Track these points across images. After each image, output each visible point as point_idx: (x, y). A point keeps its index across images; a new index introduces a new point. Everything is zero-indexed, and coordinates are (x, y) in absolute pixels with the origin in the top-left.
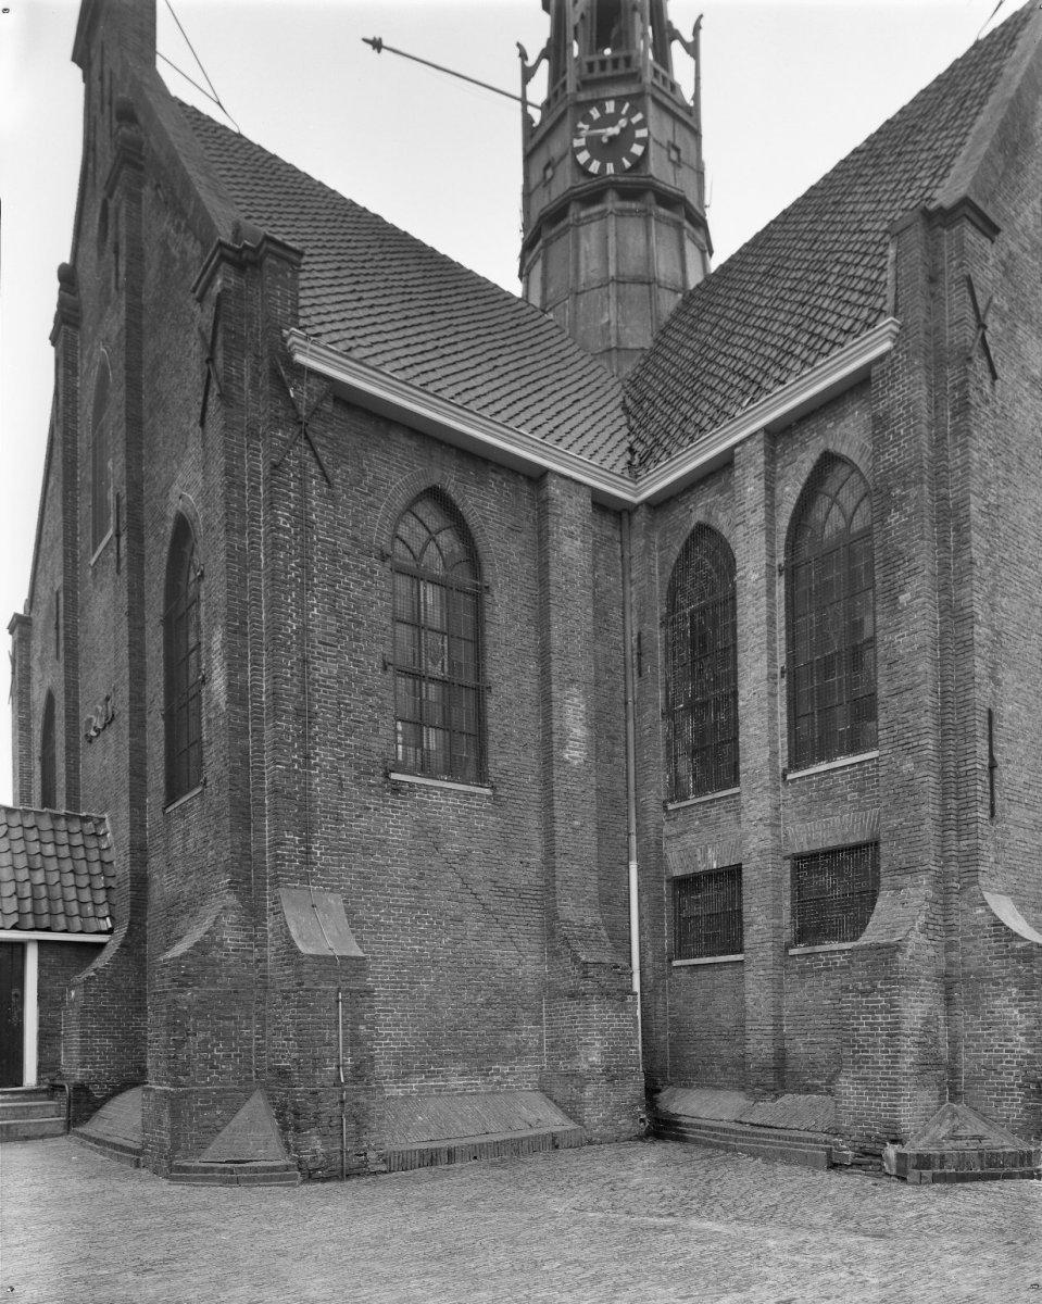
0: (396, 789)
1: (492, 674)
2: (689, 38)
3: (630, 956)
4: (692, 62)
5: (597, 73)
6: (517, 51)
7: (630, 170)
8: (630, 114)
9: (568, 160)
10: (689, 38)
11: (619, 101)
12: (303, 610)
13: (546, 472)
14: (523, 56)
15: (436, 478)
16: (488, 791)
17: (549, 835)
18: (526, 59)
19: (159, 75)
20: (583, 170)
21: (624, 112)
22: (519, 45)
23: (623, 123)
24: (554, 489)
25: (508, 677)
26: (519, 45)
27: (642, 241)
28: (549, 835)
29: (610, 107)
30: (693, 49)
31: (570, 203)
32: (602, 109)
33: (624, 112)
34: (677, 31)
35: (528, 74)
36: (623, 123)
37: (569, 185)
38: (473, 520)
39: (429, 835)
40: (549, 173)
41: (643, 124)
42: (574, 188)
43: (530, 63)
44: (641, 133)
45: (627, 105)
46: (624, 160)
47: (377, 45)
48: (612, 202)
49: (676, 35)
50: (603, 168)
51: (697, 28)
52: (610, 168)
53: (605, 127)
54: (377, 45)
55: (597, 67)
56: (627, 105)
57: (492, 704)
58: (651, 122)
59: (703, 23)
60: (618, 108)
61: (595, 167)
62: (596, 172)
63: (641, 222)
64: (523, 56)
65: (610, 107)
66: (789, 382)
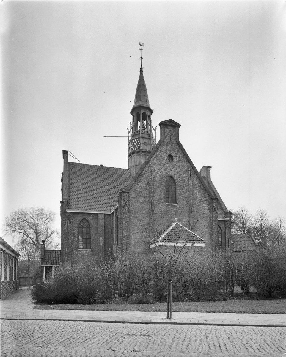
0: (79, 251)
1: (91, 237)
4: (155, 133)
7: (138, 149)
8: (138, 140)
11: (137, 139)
12: (67, 235)
15: (84, 217)
19: (181, 144)
24: (99, 215)
25: (93, 237)
27: (139, 159)
32: (134, 140)
38: (89, 221)
39: (83, 255)
41: (140, 142)
44: (139, 143)
47: (105, 137)
48: (135, 154)
49: (153, 127)
50: (135, 149)
51: (156, 128)
54: (105, 137)
57: (91, 240)
58: (141, 141)
59: (157, 127)
60: (136, 140)
63: (139, 156)
65: (135, 140)
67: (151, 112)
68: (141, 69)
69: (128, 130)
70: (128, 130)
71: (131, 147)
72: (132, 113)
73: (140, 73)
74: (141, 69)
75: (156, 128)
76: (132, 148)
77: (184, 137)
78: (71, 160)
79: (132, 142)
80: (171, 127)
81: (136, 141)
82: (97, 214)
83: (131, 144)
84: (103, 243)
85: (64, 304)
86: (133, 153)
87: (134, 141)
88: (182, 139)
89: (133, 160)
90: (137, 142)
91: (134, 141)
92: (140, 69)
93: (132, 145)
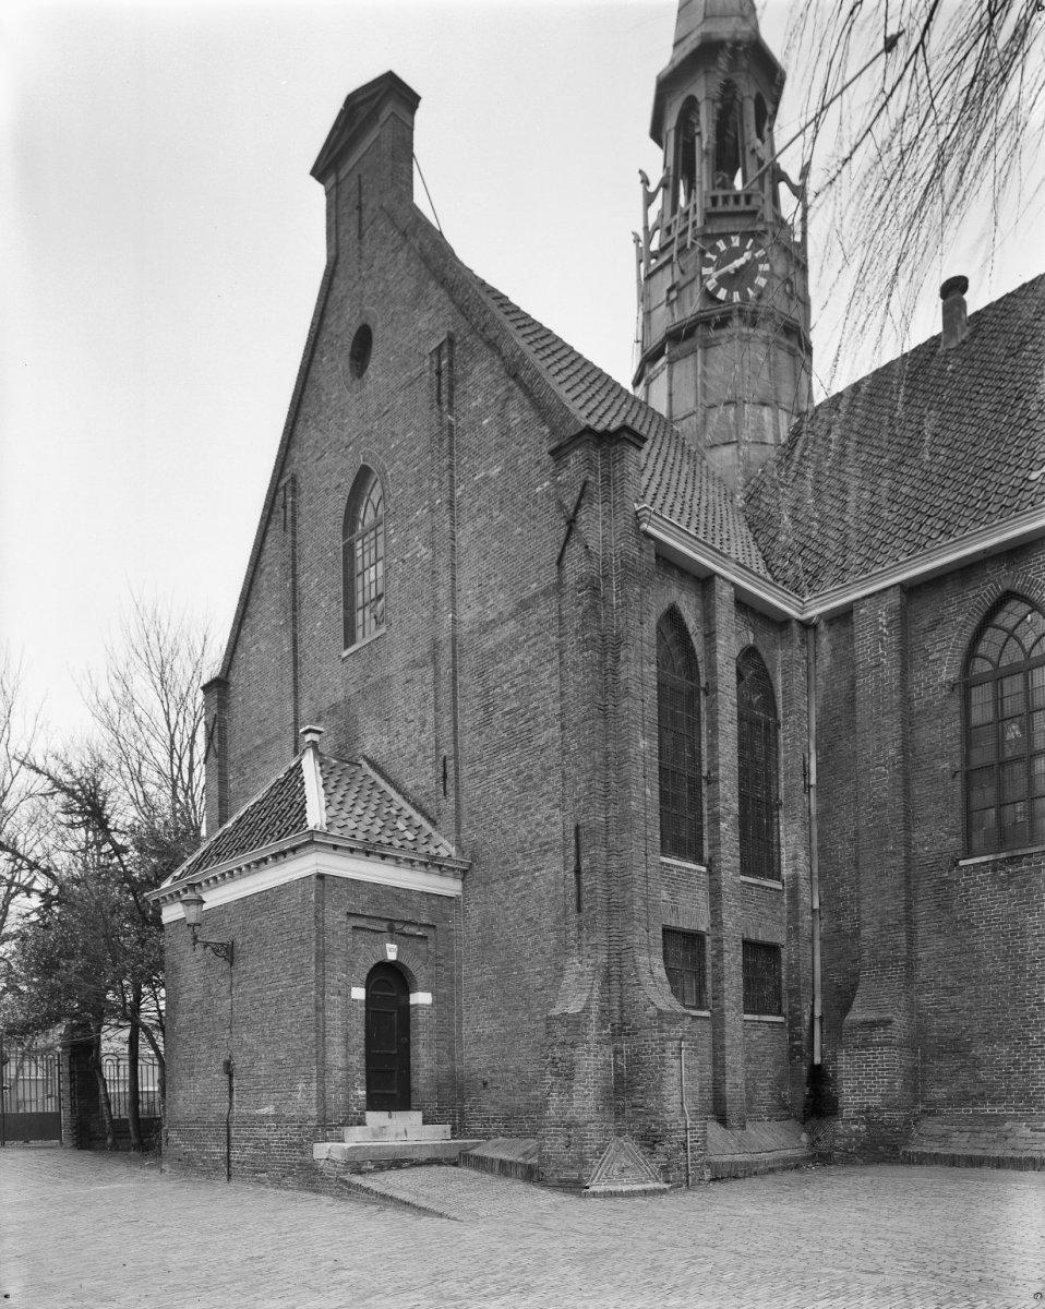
2: (795, 179)
3: (428, 894)
5: (720, 207)
6: (639, 178)
9: (697, 287)
10: (796, 180)
13: (715, 574)
14: (646, 182)
16: (704, 869)
17: (296, 711)
18: (648, 184)
20: (710, 296)
21: (748, 247)
22: (641, 172)
23: (747, 255)
26: (641, 172)
28: (296, 711)
29: (736, 241)
30: (799, 192)
31: (696, 327)
32: (728, 242)
33: (748, 247)
34: (785, 174)
35: (649, 199)
36: (747, 255)
37: (697, 309)
40: (674, 295)
41: (763, 260)
42: (703, 311)
43: (652, 189)
45: (751, 241)
46: (749, 290)
49: (784, 177)
52: (736, 297)
53: (732, 262)
55: (731, 201)
56: (751, 241)
61: (722, 294)
62: (723, 298)
64: (646, 182)
65: (736, 241)
66: (887, 566)
91: (721, 245)
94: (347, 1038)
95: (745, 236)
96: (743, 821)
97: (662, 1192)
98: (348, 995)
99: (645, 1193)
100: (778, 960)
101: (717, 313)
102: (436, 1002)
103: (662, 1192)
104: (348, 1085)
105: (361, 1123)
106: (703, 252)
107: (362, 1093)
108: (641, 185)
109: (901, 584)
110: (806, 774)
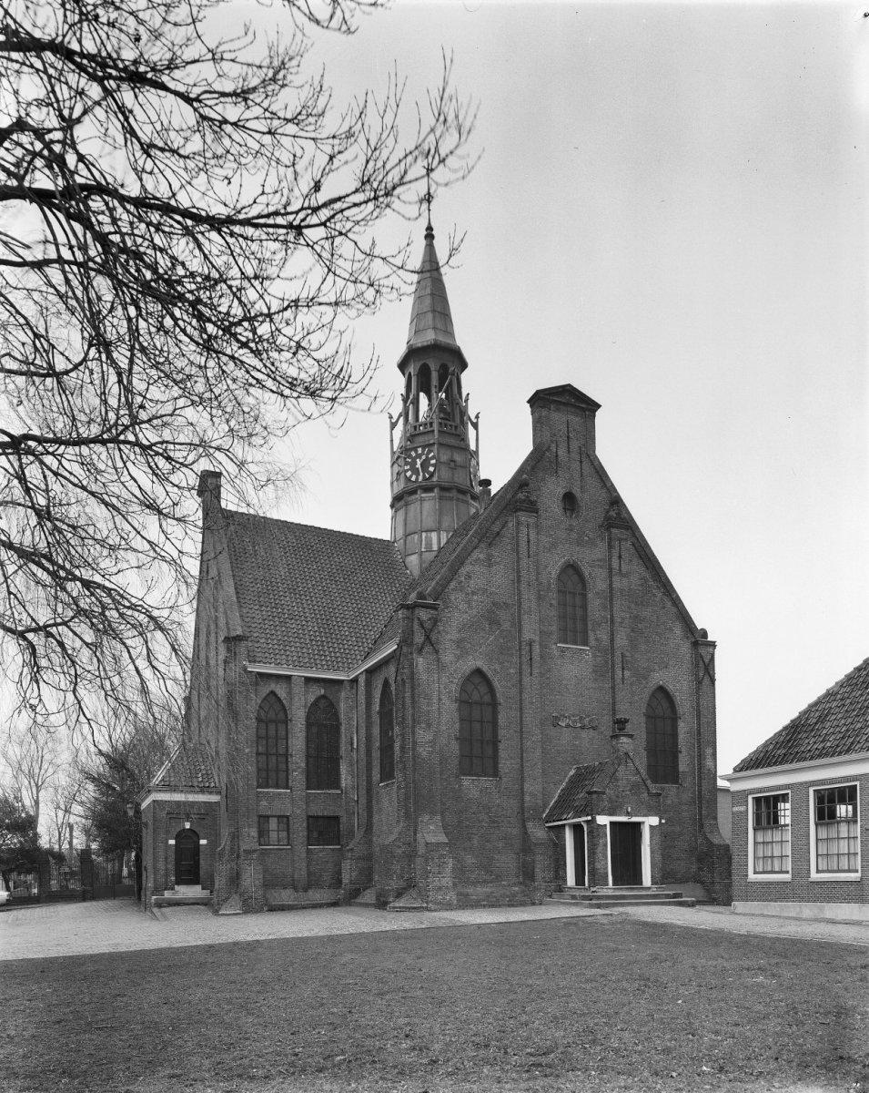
8: (428, 453)
29: (420, 450)
32: (416, 452)
35: (393, 425)
51: (477, 417)
60: (423, 451)
65: (420, 450)
67: (464, 365)
68: (430, 228)
69: (391, 417)
70: (391, 417)
71: (408, 470)
72: (402, 366)
73: (423, 242)
74: (430, 228)
75: (477, 417)
76: (409, 474)
77: (614, 446)
78: (229, 501)
79: (410, 456)
80: (565, 411)
81: (423, 453)
82: (289, 677)
83: (406, 463)
84: (705, 759)
85: (104, 954)
86: (413, 492)
87: (413, 454)
88: (606, 451)
89: (411, 514)
90: (424, 457)
91: (413, 454)
92: (427, 229)
93: (408, 467)
94: (166, 858)
95: (424, 447)
96: (381, 749)
97: (239, 914)
98: (167, 842)
99: (234, 914)
100: (339, 823)
101: (411, 486)
102: (176, 845)
103: (239, 914)
104: (167, 875)
105: (173, 889)
106: (405, 458)
107: (173, 878)
108: (464, 339)
109: (366, 670)
110: (352, 744)
